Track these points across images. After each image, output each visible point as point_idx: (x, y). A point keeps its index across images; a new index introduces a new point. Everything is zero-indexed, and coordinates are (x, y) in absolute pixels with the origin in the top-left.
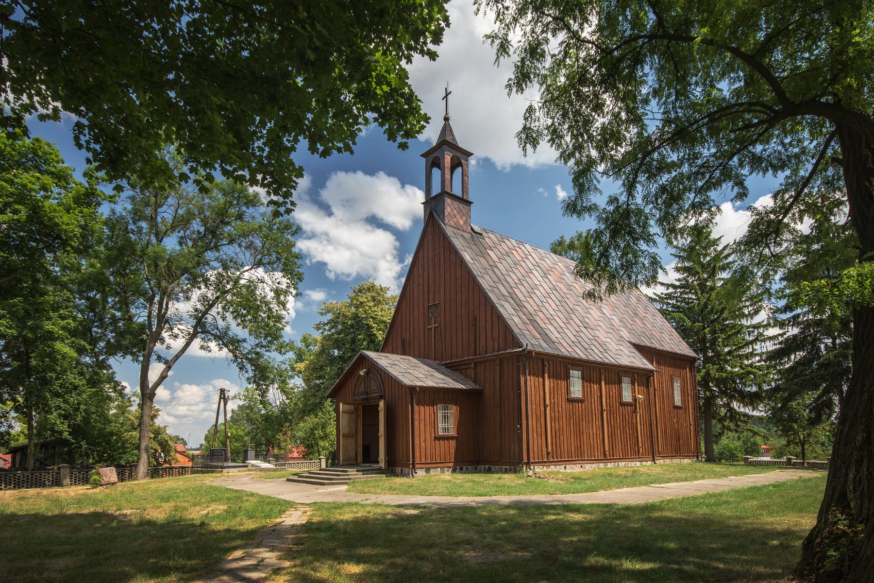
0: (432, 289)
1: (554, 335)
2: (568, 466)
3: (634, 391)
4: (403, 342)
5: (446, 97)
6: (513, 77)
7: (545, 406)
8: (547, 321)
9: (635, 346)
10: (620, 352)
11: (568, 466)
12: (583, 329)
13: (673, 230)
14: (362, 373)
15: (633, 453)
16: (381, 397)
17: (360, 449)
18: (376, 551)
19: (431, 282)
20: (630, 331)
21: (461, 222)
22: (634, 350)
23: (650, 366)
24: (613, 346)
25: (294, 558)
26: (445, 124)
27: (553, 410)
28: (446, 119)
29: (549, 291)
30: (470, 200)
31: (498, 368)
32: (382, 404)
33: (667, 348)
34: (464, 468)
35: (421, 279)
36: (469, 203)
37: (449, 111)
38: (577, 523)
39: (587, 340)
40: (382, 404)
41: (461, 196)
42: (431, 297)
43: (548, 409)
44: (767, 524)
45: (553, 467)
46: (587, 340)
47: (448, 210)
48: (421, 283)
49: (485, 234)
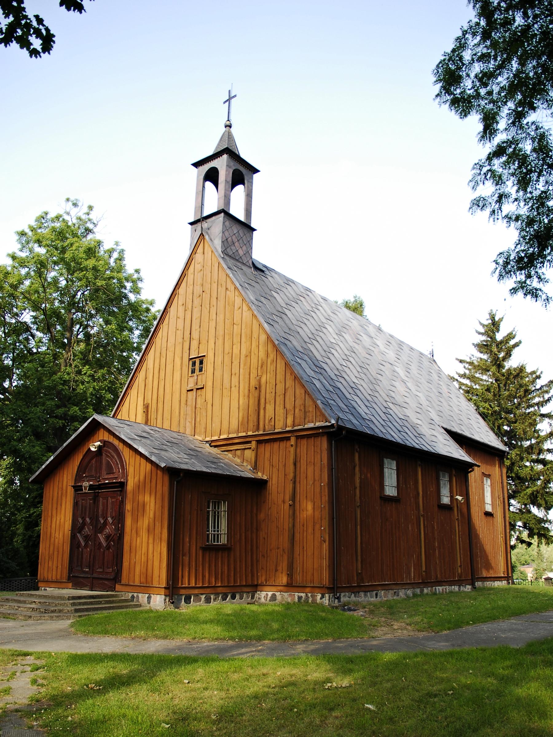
0: (195, 335)
1: (362, 410)
3: (451, 491)
5: (229, 100)
8: (351, 391)
9: (446, 430)
10: (434, 439)
12: (391, 405)
13: (535, 518)
19: (195, 327)
20: (440, 413)
21: (241, 252)
22: (448, 437)
23: (467, 458)
24: (425, 429)
25: (350, 671)
29: (347, 353)
30: (253, 225)
33: (477, 437)
35: (180, 322)
37: (231, 118)
38: (375, 645)
39: (351, 366)
41: (242, 218)
42: (195, 344)
44: (392, 611)
46: (351, 366)
48: (180, 326)
49: (267, 272)
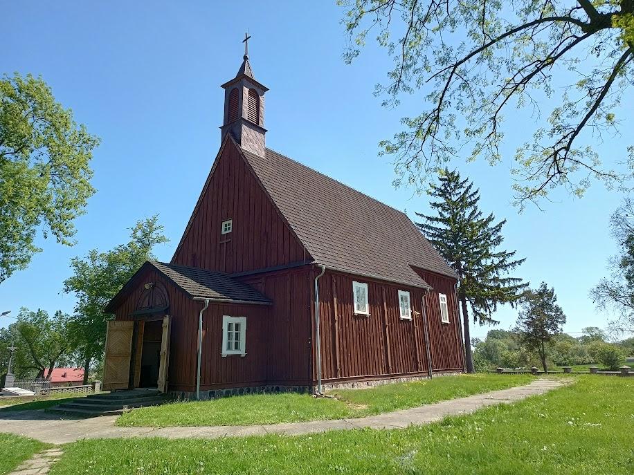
2: (370, 383)
4: (194, 256)
6: (563, 333)
7: (385, 327)
11: (370, 383)
14: (147, 287)
15: (413, 367)
16: (167, 312)
17: (138, 373)
18: (363, 422)
26: (244, 62)
27: (341, 325)
28: (245, 58)
31: (288, 283)
32: (166, 320)
34: (251, 389)
36: (263, 131)
37: (248, 51)
40: (166, 320)
43: (336, 324)
45: (341, 385)
47: (244, 134)
